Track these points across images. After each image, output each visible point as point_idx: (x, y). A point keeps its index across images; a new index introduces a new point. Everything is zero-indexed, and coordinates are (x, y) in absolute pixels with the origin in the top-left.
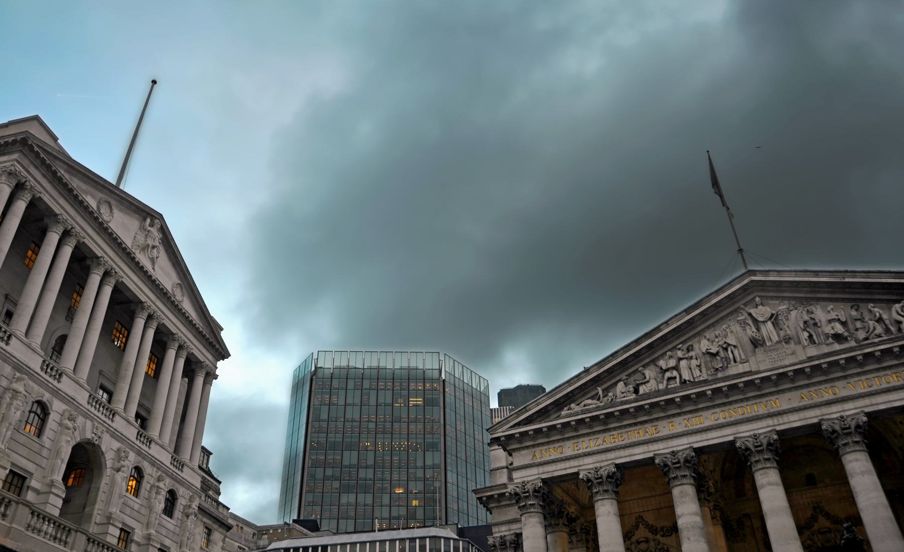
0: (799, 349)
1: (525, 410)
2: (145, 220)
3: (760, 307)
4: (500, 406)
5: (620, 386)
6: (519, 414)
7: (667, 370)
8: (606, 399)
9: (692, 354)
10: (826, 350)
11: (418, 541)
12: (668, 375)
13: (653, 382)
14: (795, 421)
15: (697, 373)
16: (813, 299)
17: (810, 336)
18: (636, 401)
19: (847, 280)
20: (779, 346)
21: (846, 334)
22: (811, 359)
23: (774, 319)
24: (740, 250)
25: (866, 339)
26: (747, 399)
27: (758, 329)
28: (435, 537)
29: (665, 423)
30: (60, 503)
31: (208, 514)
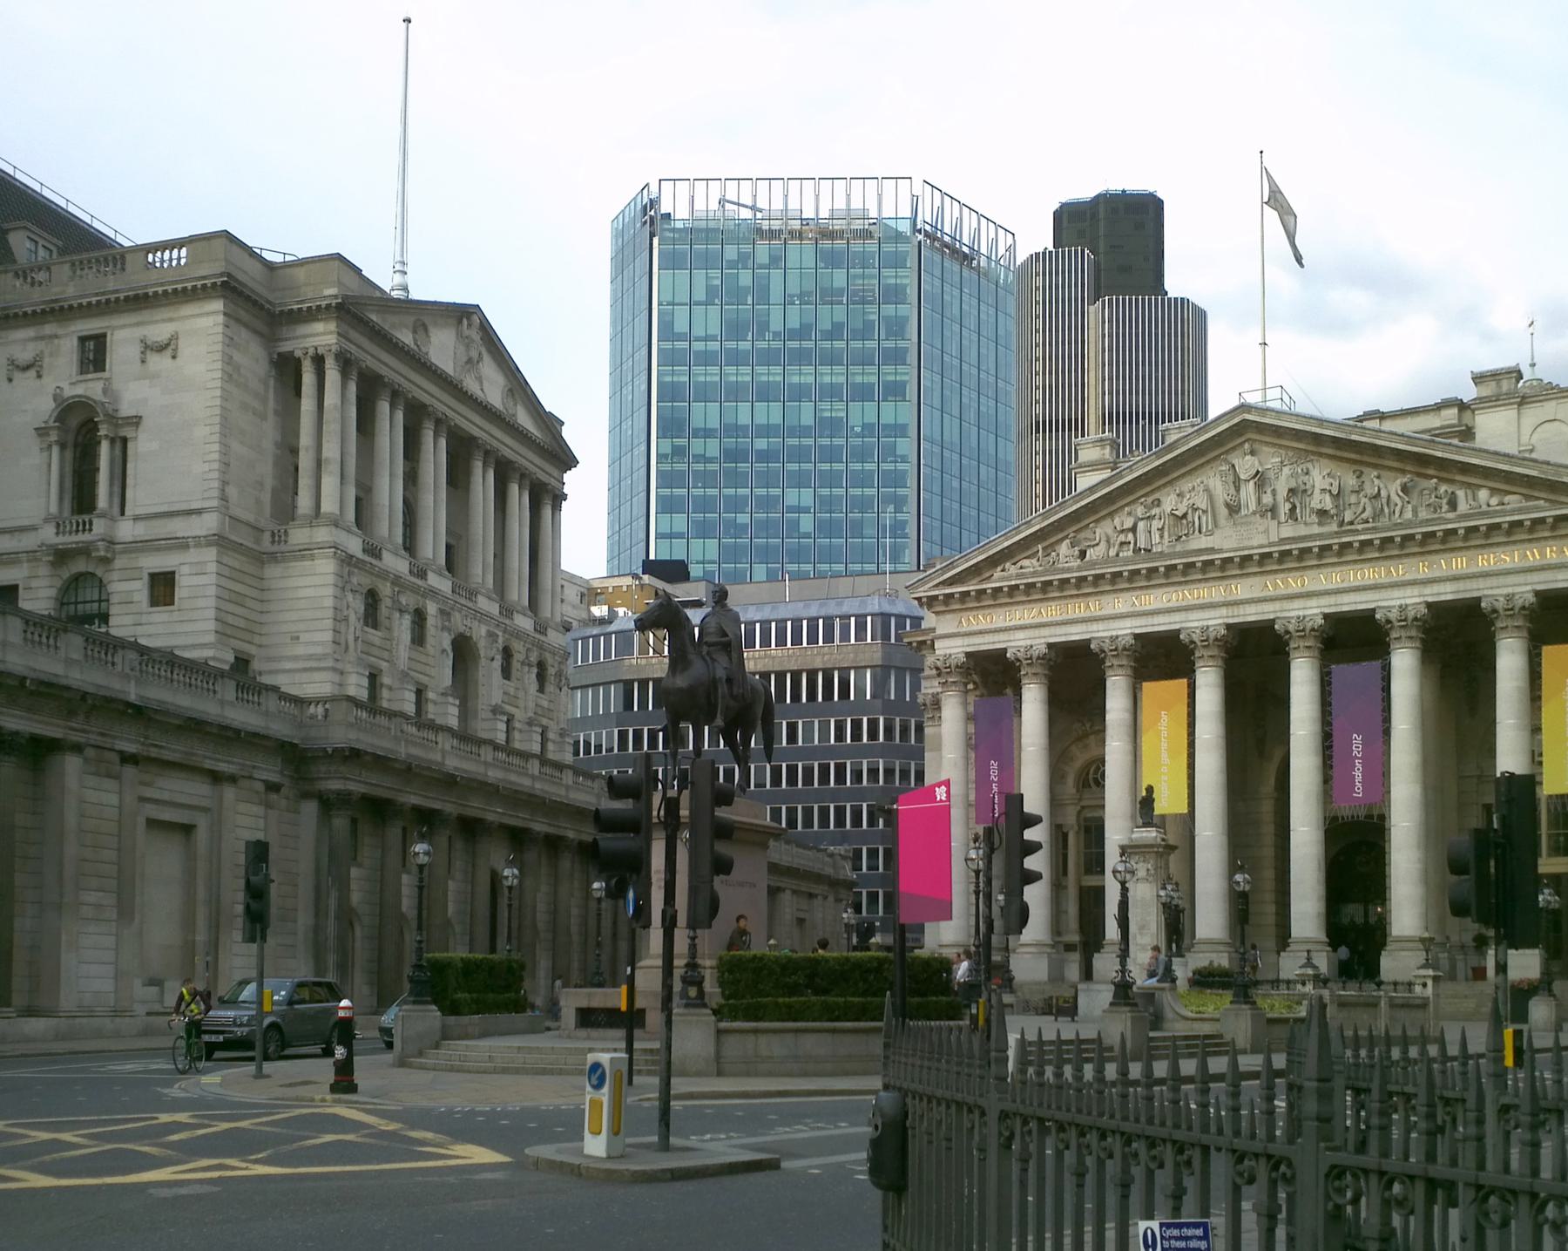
1: (951, 566)
2: (460, 322)
5: (1064, 548)
7: (1122, 531)
10: (1302, 531)
12: (1122, 538)
14: (1251, 614)
15: (1156, 538)
16: (1313, 453)
17: (1294, 508)
18: (1079, 569)
19: (1353, 437)
20: (1252, 519)
22: (1283, 541)
23: (1260, 479)
25: (1351, 523)
27: (1238, 489)
28: (882, 614)
30: (456, 711)
31: (248, 298)
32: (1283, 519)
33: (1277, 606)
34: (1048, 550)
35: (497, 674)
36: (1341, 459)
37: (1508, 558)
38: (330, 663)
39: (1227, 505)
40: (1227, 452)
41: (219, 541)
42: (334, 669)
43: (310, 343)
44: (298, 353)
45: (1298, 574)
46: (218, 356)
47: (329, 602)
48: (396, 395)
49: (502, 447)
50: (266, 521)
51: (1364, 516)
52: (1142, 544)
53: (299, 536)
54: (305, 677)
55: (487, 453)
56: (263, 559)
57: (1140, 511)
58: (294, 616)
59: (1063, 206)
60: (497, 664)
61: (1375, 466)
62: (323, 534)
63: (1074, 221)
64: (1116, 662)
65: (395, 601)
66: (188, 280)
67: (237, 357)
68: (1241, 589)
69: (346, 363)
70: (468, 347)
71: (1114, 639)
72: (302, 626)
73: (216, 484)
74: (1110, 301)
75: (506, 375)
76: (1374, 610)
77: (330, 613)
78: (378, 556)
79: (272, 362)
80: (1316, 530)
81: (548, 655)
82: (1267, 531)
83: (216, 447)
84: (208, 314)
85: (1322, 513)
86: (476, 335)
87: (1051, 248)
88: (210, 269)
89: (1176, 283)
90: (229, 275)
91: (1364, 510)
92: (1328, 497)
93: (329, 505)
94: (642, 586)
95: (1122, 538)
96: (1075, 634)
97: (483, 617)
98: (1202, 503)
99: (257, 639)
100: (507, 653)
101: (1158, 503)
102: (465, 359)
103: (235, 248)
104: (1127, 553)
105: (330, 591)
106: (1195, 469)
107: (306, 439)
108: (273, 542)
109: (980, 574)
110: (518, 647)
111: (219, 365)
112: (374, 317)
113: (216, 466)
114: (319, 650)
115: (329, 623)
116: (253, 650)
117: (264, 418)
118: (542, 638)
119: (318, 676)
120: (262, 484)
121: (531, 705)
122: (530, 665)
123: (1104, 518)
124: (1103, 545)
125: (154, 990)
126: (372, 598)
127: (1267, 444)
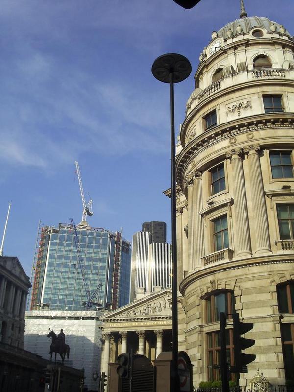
5: (131, 312)
37: (123, 325)
48: (21, 289)
49: (9, 277)
96: (133, 329)
97: (9, 317)
100: (13, 325)
125: (278, 244)
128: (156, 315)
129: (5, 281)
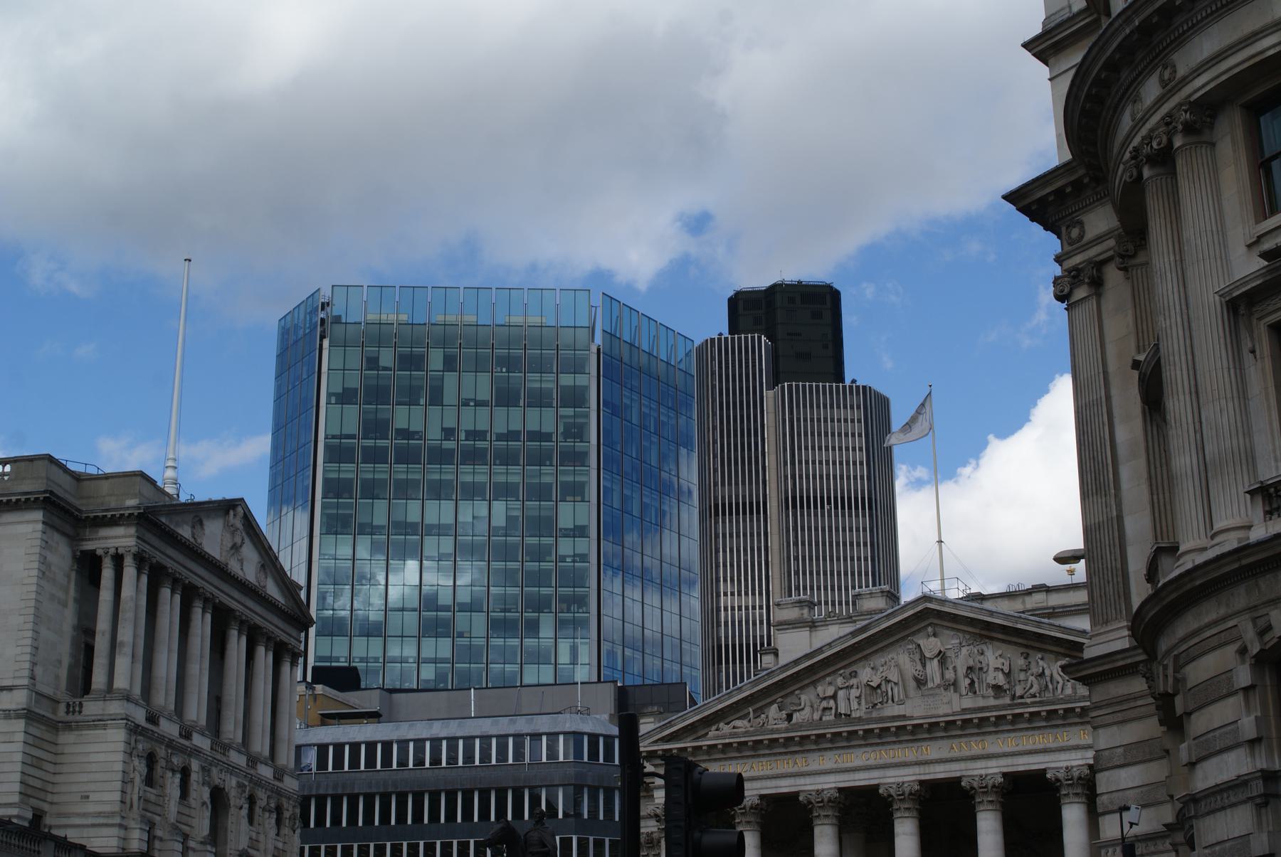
0: (955, 697)
1: (670, 724)
3: (932, 639)
4: (733, 330)
6: (662, 728)
7: (824, 698)
8: (758, 720)
9: (853, 681)
10: (981, 703)
11: (544, 738)
12: (824, 704)
13: (808, 710)
14: (940, 772)
15: (854, 705)
18: (787, 730)
19: (1019, 626)
20: (937, 691)
21: (1006, 687)
22: (964, 711)
23: (942, 657)
24: (940, 542)
25: (1022, 697)
26: (900, 742)
27: (924, 666)
28: (574, 733)
29: (815, 755)
31: (62, 509)
32: (964, 692)
33: (962, 765)
34: (759, 712)
35: (245, 821)
36: (1009, 643)
38: (117, 820)
39: (916, 679)
40: (913, 633)
41: (29, 715)
42: (120, 826)
43: (111, 544)
44: (99, 552)
45: (979, 738)
46: (36, 557)
47: (119, 767)
48: (270, 639)
50: (62, 693)
51: (1032, 691)
52: (842, 710)
53: (92, 708)
54: (92, 832)
55: (242, 622)
56: (56, 726)
57: (840, 681)
58: (83, 778)
59: (738, 294)
60: (244, 812)
61: (1040, 650)
62: (115, 708)
63: (748, 309)
64: (822, 813)
65: (168, 761)
66: (14, 494)
67: (51, 558)
68: (933, 750)
69: (140, 559)
70: (233, 533)
71: (819, 792)
72: (92, 787)
73: (27, 665)
74: (790, 387)
75: (260, 553)
76: (1045, 770)
77: (119, 776)
78: (280, 780)
79: (74, 557)
80: (992, 702)
81: (284, 801)
82: (949, 703)
83: (30, 634)
84: (28, 522)
85: (997, 688)
86: (238, 523)
87: (726, 334)
88: (32, 485)
89: (856, 369)
90: (51, 492)
91: (1032, 686)
92: (1000, 675)
93: (120, 682)
94: (315, 697)
95: (824, 704)
96: (785, 786)
97: (232, 769)
98: (894, 677)
99: (49, 798)
100: (252, 800)
101: (854, 674)
102: (230, 545)
103: (54, 468)
104: (829, 717)
105: (120, 757)
106: (887, 646)
107: (103, 624)
108: (67, 713)
109: (696, 732)
110: (261, 795)
111: (36, 565)
112: (163, 520)
113: (28, 650)
114: (107, 808)
115: (118, 785)
116: (46, 807)
117: (65, 605)
118: (252, 772)
119: (105, 831)
120: (60, 662)
121: (270, 847)
122: (270, 811)
123: (807, 685)
124: (808, 710)
126: (151, 759)
127: (948, 628)
128: (882, 720)
129: (204, 611)
